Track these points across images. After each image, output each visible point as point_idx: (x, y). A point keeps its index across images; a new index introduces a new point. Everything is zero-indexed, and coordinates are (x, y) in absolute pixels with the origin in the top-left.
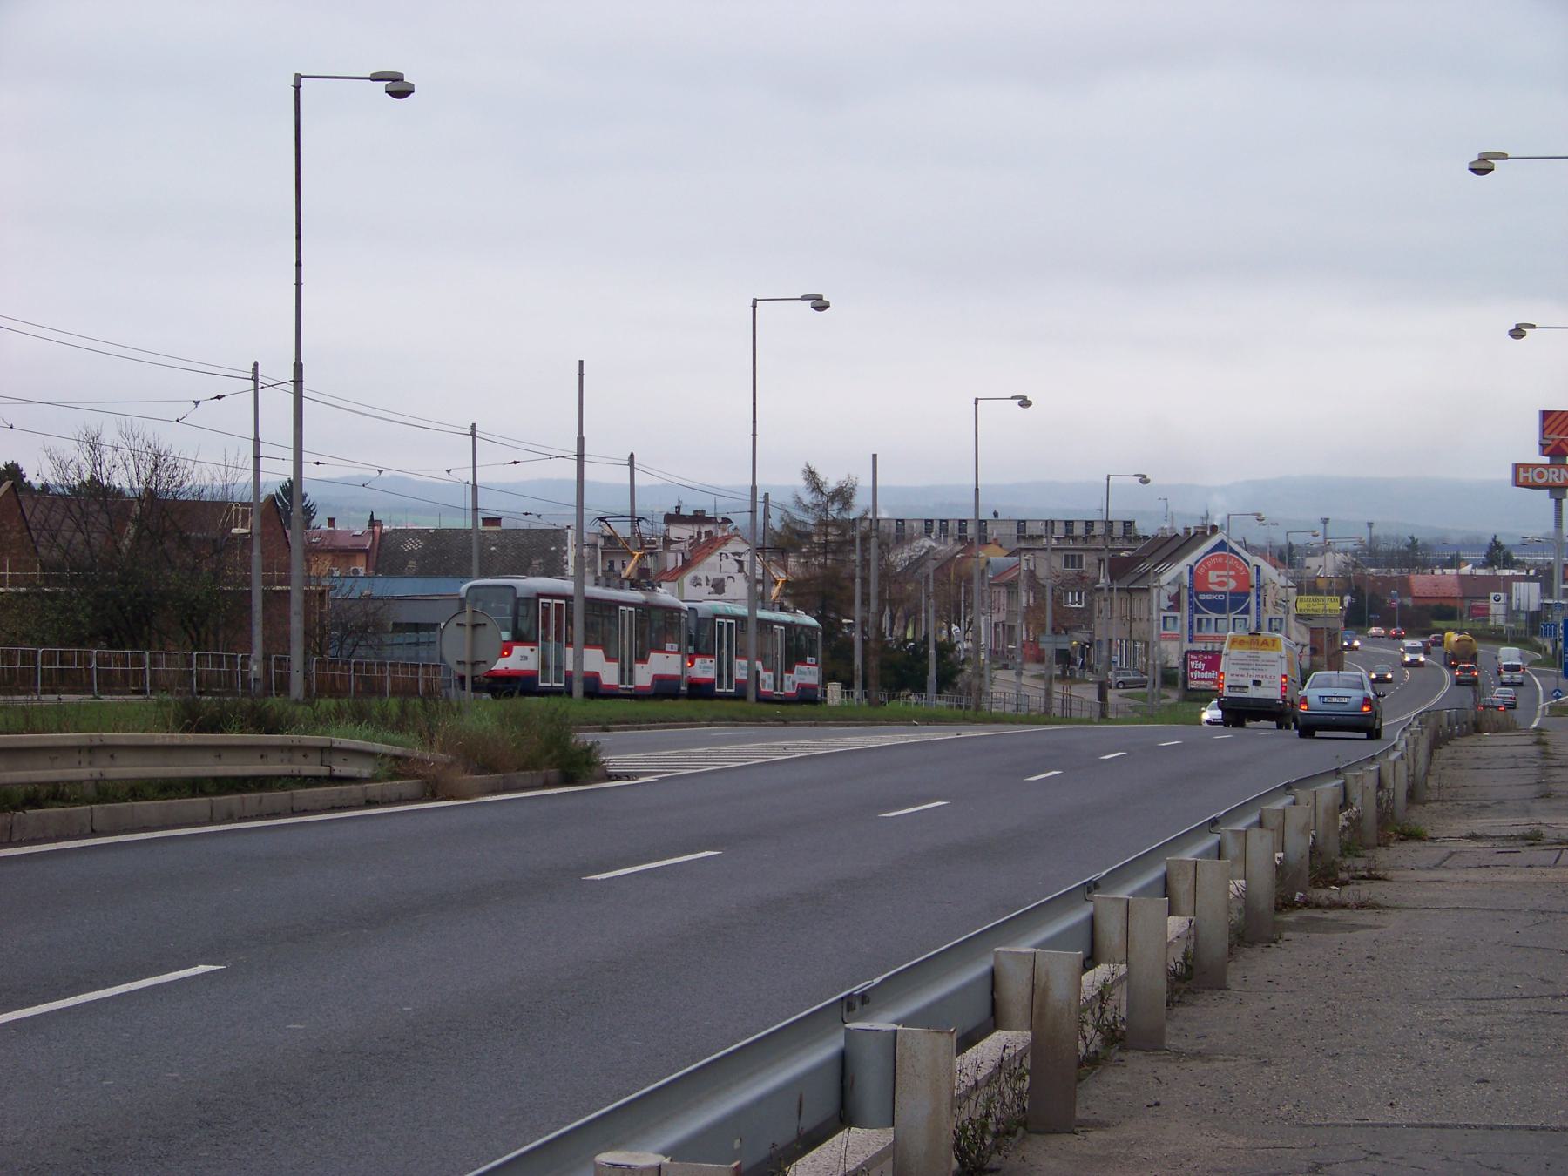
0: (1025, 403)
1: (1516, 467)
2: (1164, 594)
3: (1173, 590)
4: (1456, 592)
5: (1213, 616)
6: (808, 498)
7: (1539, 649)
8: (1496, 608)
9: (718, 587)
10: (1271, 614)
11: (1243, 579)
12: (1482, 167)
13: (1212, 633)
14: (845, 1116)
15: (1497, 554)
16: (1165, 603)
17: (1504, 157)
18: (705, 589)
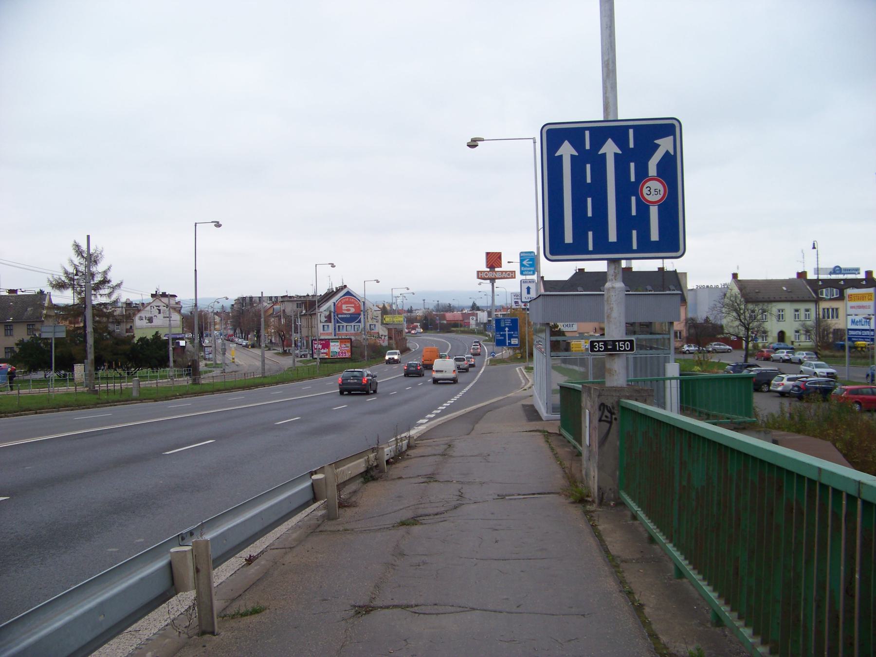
0: (378, 282)
1: (478, 272)
2: (323, 315)
3: (327, 313)
4: (461, 318)
5: (345, 324)
6: (77, 260)
7: (486, 336)
8: (472, 322)
9: (150, 320)
10: (370, 322)
11: (357, 307)
12: (473, 144)
13: (345, 332)
14: (315, 499)
15: (475, 308)
16: (323, 319)
17: (482, 140)
18: (145, 322)
